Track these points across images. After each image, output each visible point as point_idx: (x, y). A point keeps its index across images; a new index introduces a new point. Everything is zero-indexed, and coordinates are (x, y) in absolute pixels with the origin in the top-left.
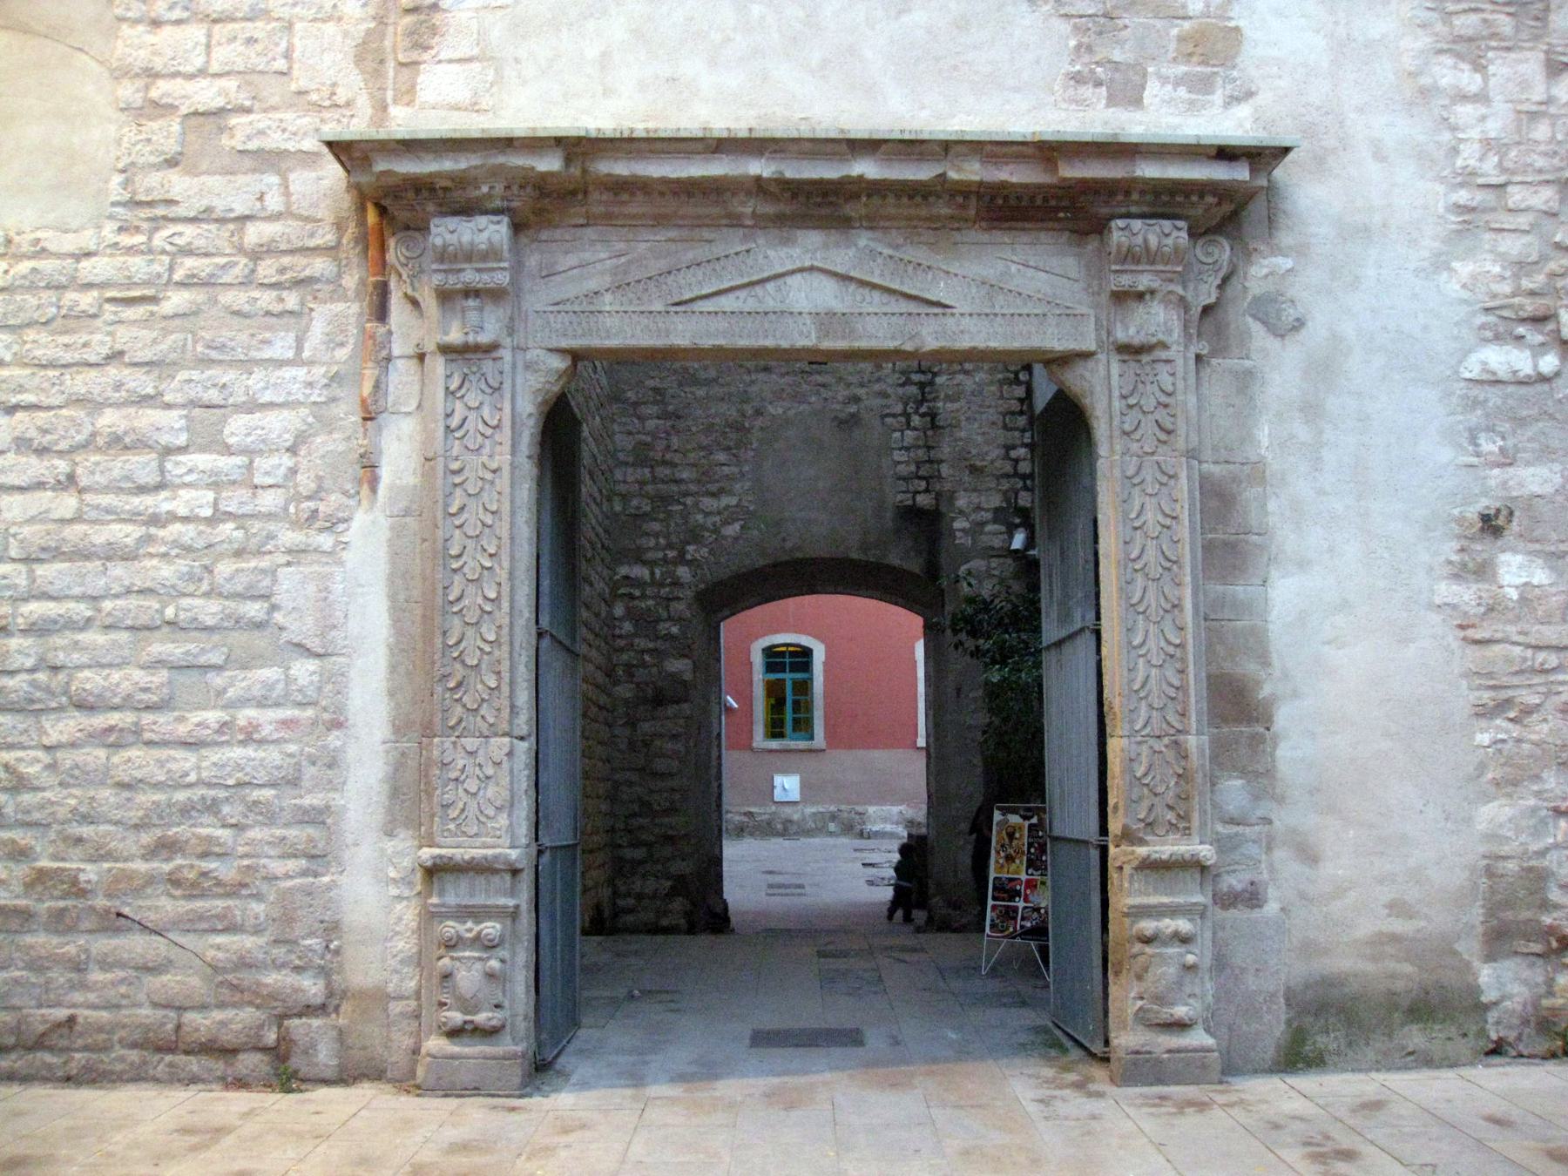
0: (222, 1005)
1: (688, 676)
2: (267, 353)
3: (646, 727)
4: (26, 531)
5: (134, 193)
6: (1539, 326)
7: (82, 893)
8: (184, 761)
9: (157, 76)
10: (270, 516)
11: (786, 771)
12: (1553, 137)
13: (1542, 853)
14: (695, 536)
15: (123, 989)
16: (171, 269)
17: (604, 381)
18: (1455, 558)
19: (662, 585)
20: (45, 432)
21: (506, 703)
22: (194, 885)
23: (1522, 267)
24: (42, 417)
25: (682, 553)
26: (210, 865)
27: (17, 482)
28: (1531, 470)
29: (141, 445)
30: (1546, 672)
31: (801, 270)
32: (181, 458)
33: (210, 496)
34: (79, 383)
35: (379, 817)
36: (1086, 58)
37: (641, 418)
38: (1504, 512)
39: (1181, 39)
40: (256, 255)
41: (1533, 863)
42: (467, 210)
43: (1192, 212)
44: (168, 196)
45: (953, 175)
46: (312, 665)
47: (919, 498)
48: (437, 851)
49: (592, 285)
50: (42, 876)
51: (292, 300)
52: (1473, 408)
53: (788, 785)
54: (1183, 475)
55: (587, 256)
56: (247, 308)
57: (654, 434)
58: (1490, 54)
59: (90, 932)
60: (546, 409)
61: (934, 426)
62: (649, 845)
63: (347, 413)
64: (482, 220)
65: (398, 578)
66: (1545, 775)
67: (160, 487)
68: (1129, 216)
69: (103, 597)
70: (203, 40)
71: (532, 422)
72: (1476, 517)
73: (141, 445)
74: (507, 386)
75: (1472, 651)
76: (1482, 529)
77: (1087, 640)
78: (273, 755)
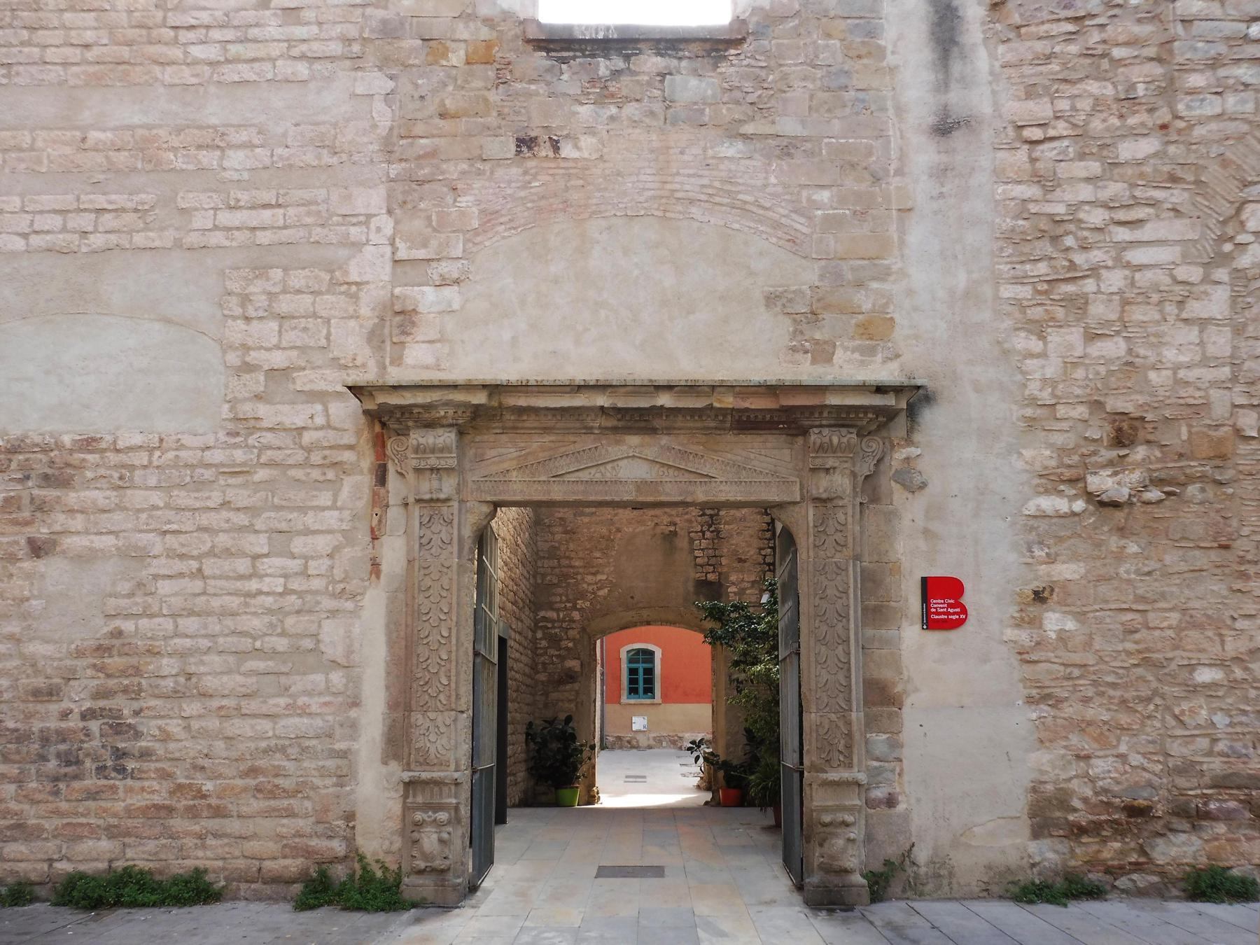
0: (285, 857)
1: (578, 669)
2: (315, 503)
3: (554, 696)
4: (173, 599)
5: (236, 413)
7: (204, 797)
10: (316, 592)
13: (1069, 780)
14: (582, 595)
15: (227, 849)
16: (259, 456)
18: (1016, 615)
20: (183, 545)
21: (453, 693)
22: (271, 792)
23: (1062, 451)
24: (182, 538)
25: (575, 605)
26: (279, 781)
28: (1066, 566)
29: (242, 554)
30: (1073, 679)
33: (282, 580)
34: (205, 519)
35: (378, 755)
36: (799, 338)
37: (553, 534)
38: (1048, 589)
39: (858, 326)
40: (309, 450)
42: (430, 425)
43: (859, 423)
45: (716, 405)
49: (506, 466)
50: (180, 787)
51: (331, 475)
53: (639, 723)
54: (851, 569)
57: (560, 543)
58: (1049, 330)
63: (363, 537)
64: (440, 431)
65: (392, 626)
67: (250, 577)
68: (821, 426)
70: (277, 328)
72: (1030, 592)
73: (242, 554)
74: (455, 522)
75: (1025, 667)
78: (319, 722)
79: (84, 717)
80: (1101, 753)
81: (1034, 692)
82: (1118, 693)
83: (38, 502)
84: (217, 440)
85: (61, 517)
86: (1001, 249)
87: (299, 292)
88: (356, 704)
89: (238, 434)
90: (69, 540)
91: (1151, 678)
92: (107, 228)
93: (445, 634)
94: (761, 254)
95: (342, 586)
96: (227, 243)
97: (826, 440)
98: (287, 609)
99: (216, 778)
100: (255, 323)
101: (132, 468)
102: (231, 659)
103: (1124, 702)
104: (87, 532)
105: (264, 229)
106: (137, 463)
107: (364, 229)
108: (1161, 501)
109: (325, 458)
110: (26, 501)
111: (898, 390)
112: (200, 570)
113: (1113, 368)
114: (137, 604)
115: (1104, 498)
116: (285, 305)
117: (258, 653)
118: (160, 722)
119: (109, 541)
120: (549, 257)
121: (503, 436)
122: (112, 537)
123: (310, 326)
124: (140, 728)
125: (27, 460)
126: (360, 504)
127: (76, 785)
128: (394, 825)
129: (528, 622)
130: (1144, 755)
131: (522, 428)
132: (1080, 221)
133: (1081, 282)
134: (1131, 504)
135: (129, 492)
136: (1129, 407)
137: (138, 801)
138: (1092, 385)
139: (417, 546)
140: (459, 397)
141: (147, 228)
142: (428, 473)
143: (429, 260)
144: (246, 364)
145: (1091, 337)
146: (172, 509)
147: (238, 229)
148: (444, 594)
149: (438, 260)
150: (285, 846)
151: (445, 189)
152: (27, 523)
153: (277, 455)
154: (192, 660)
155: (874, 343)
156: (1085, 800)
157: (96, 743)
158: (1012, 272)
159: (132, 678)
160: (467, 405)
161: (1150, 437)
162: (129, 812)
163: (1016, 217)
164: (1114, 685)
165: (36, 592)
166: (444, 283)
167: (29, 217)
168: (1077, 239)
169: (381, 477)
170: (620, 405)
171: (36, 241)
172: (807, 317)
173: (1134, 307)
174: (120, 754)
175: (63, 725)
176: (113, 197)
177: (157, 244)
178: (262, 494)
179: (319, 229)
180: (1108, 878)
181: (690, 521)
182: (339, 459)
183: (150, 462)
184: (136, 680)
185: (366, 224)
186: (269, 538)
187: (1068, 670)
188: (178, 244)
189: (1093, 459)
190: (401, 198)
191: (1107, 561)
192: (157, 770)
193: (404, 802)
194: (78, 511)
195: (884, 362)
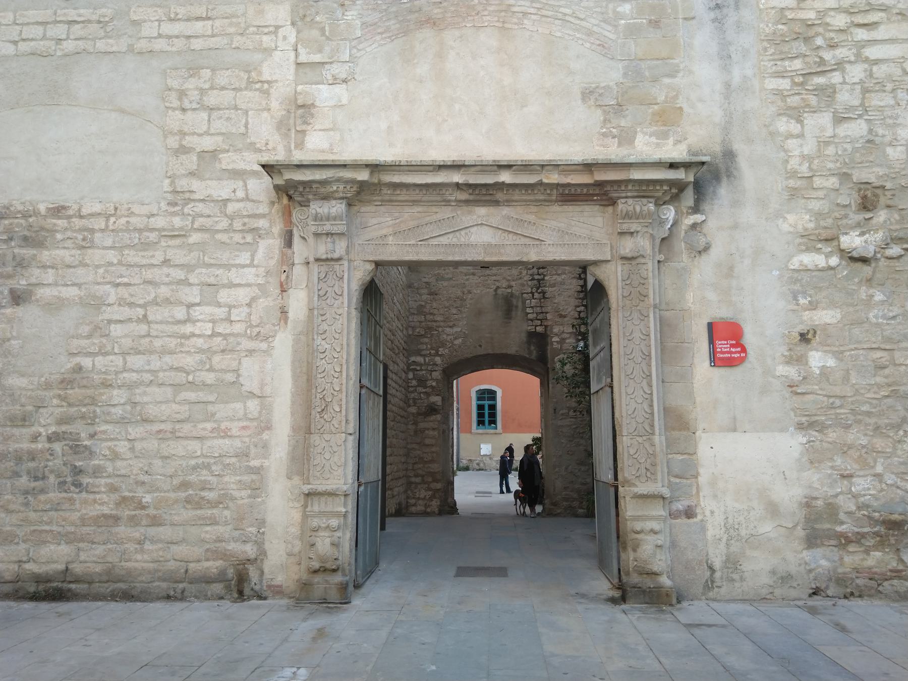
0: (207, 560)
2: (237, 262)
4: (123, 340)
5: (175, 187)
6: (828, 243)
7: (144, 508)
8: (194, 446)
9: (185, 134)
11: (485, 443)
12: (837, 153)
13: (836, 496)
14: (443, 345)
15: (161, 553)
16: (193, 223)
17: (404, 279)
18: (786, 353)
19: (428, 365)
20: (132, 296)
21: (344, 419)
22: (198, 503)
23: (819, 215)
24: (131, 289)
25: (437, 352)
26: (205, 494)
27: (118, 318)
28: (825, 312)
31: (477, 225)
32: (197, 308)
33: (211, 325)
34: (149, 274)
38: (812, 332)
39: (654, 114)
40: (231, 218)
41: (830, 501)
42: (326, 198)
43: (657, 194)
44: (191, 189)
45: (545, 181)
46: (256, 402)
47: (538, 328)
48: (310, 487)
49: (384, 232)
50: (124, 499)
51: (249, 238)
52: (795, 283)
54: (651, 315)
55: (383, 220)
56: (228, 241)
58: (805, 115)
59: (147, 526)
60: (364, 287)
61: (544, 298)
62: (423, 476)
63: (275, 290)
66: (835, 458)
67: (185, 322)
68: (626, 197)
69: (158, 371)
70: (207, 118)
71: (357, 293)
74: (346, 277)
76: (800, 340)
77: (608, 390)
79: (49, 439)
80: (861, 473)
81: (804, 419)
82: (872, 421)
83: (18, 259)
84: (160, 208)
85: (37, 272)
86: (765, 49)
87: (223, 88)
88: (269, 428)
89: (176, 204)
90: (42, 291)
91: (900, 408)
92: (77, 36)
93: (338, 369)
94: (578, 57)
95: (258, 329)
96: (169, 49)
97: (631, 208)
98: (214, 349)
99: (154, 491)
100: (189, 112)
101: (92, 231)
102: (169, 390)
103: (877, 428)
104: (56, 284)
105: (197, 37)
106: (96, 227)
107: (273, 37)
108: (901, 256)
109: (244, 224)
110: (9, 258)
111: (687, 166)
112: (145, 316)
113: (857, 145)
114: (94, 344)
115: (855, 254)
116: (212, 99)
117: (192, 385)
118: (109, 444)
119: (73, 292)
120: (415, 61)
121: (382, 208)
122: (76, 288)
123: (233, 116)
124: (94, 449)
125: (11, 224)
126: (273, 262)
127: (42, 497)
128: (295, 530)
129: (402, 365)
130: (897, 474)
131: (396, 201)
132: (828, 24)
133: (829, 75)
134: (877, 260)
135: (90, 251)
136: (873, 179)
137: (93, 511)
138: (841, 159)
139: (316, 298)
140: (348, 174)
141: (107, 36)
142: (324, 237)
143: (323, 63)
144: (182, 146)
145: (839, 120)
146: (124, 265)
147: (177, 37)
148: (337, 336)
149: (331, 63)
150: (207, 550)
151: (335, 5)
152: (9, 277)
153: (207, 222)
154: (137, 391)
155: (665, 128)
156: (849, 513)
157: (58, 462)
158: (774, 68)
159: (89, 407)
160: (353, 181)
161: (890, 202)
162: (83, 521)
163: (777, 22)
164: (868, 414)
165: (14, 334)
166: (336, 81)
167: (18, 28)
168: (825, 39)
169: (289, 242)
170: (471, 182)
171: (23, 47)
172: (614, 106)
173: (873, 95)
174: (78, 471)
175: (33, 446)
176: (82, 11)
177: (114, 49)
178: (195, 254)
179: (239, 38)
180: (873, 584)
181: (523, 285)
182: (256, 225)
183: (107, 226)
184: (92, 408)
185: (275, 33)
186: (201, 290)
187: (831, 400)
188: (131, 49)
189: (844, 221)
190: (301, 12)
191: (858, 308)
192: (106, 484)
193: (305, 512)
194: (49, 267)
195: (675, 144)
